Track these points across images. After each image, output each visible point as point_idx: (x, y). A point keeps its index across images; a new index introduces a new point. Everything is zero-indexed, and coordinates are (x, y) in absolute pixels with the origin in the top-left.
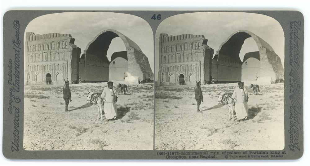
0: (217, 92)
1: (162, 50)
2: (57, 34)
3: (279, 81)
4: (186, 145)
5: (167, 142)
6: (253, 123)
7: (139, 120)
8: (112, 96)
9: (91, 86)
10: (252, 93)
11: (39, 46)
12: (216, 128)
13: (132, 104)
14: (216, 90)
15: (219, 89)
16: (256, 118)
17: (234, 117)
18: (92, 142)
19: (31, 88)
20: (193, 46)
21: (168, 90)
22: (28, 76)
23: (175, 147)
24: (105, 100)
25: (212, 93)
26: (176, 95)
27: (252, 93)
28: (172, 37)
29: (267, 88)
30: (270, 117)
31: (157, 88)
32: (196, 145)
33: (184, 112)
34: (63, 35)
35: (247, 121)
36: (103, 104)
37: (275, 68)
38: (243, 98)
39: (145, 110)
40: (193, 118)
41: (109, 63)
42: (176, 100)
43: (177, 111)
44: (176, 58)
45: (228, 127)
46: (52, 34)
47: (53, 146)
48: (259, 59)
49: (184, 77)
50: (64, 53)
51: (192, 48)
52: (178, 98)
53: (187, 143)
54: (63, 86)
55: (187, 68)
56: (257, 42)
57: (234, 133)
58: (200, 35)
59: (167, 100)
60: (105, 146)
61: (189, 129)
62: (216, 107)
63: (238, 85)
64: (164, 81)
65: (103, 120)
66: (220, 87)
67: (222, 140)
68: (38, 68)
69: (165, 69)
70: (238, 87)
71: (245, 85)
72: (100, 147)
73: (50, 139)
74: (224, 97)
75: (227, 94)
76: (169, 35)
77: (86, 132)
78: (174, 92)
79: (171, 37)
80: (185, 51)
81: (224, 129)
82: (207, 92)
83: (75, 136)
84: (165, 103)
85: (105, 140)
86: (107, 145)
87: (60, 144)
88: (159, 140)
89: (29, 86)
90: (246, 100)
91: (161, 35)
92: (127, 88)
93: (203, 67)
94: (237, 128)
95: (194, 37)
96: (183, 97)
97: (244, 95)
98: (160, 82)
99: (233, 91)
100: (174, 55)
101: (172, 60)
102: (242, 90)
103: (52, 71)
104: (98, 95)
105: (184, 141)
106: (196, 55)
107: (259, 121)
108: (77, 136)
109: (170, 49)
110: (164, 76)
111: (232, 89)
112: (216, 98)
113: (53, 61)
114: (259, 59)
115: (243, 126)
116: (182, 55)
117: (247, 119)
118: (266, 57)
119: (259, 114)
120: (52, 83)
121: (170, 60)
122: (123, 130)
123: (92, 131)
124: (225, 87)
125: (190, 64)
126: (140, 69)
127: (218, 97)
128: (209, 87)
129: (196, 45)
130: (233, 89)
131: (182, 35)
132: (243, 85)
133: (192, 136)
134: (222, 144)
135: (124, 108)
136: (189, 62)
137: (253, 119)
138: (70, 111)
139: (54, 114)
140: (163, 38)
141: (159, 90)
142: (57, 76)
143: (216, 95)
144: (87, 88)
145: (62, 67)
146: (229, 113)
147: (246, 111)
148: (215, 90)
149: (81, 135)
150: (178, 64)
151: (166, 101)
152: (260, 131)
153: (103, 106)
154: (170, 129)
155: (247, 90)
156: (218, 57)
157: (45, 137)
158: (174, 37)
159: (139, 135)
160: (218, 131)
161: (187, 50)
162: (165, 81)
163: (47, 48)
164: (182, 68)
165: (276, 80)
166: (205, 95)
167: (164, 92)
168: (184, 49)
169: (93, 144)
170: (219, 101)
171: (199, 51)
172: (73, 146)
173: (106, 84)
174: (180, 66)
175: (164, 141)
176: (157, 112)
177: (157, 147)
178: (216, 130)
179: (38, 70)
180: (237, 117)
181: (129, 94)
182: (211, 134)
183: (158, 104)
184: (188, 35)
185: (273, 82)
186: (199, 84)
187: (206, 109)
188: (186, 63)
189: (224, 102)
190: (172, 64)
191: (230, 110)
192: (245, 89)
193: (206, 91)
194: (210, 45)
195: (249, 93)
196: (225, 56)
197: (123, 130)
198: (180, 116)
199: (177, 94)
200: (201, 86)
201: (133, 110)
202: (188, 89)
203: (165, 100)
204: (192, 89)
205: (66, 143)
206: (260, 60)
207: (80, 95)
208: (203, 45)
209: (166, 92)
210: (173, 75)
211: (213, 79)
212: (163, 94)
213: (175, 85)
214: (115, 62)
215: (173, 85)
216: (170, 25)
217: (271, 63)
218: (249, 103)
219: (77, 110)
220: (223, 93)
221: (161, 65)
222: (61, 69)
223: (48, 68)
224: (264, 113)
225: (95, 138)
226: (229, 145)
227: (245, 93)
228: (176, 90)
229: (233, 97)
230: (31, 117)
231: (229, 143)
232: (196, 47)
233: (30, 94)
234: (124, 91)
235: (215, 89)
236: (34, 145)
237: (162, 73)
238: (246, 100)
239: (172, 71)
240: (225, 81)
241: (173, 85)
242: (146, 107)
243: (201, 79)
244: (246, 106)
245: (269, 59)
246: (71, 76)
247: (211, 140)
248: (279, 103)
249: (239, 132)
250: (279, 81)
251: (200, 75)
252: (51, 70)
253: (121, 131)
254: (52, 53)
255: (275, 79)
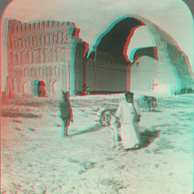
0: (94, 108)
1: (11, 44)
2: (54, 23)
3: (186, 91)
4: (47, 186)
5: (19, 182)
6: (147, 155)
7: (173, 150)
8: (132, 113)
9: (103, 99)
10: (145, 110)
11: (27, 40)
12: (92, 162)
13: (164, 126)
14: (93, 105)
15: (96, 103)
16: (153, 146)
17: (120, 145)
18: (102, 183)
19: (15, 102)
20: (58, 38)
21: (20, 104)
22: (11, 84)
23: (32, 190)
24: (122, 119)
25: (87, 109)
26: (33, 112)
27: (145, 110)
28: (27, 25)
29: (36, 103)
30: (172, 144)
31: (5, 101)
32: (63, 187)
33: (44, 137)
34: (63, 24)
35: (138, 150)
36: (119, 126)
37: (180, 71)
38: (132, 116)
39: (182, 134)
40: (57, 146)
41: (129, 64)
42: (32, 120)
43: (33, 136)
44: (33, 57)
45: (111, 159)
46: (38, 24)
47: (44, 189)
48: (157, 59)
49: (44, 85)
50: (64, 50)
51: (57, 42)
52: (36, 117)
53: (48, 184)
54: (60, 99)
55: (49, 72)
56: (153, 34)
57: (119, 169)
58: (68, 23)
59: (19, 119)
60: (121, 188)
61: (51, 162)
62: (92, 130)
63: (125, 97)
64: (15, 91)
65: (120, 150)
66: (99, 99)
67: (101, 179)
68: (25, 73)
69: (16, 72)
70: (125, 100)
71: (135, 97)
72: (114, 189)
73: (40, 179)
74: (104, 115)
75: (108, 110)
76: (22, 23)
77: (93, 167)
78: (29, 108)
79: (25, 25)
80: (46, 47)
81: (104, 163)
82: (79, 107)
83: (77, 173)
84: (16, 123)
85: (122, 179)
86: (125, 186)
87: (55, 186)
88: (8, 180)
89: (13, 100)
90: (137, 119)
91: (10, 22)
92: (157, 103)
93: (73, 70)
94: (124, 161)
95: (59, 26)
96: (42, 114)
97: (133, 111)
98: (9, 92)
99: (118, 106)
100: (30, 52)
101: (27, 60)
102: (130, 105)
103: (46, 77)
104: (111, 112)
105: (45, 180)
106: (62, 51)
107: (157, 151)
108: (80, 173)
109: (24, 43)
110: (15, 83)
111: (116, 104)
112: (91, 116)
113: (47, 63)
114: (157, 59)
115: (133, 158)
116: (41, 52)
117: (138, 148)
118: (167, 54)
119: (157, 140)
120: (46, 95)
121: (24, 60)
122: (149, 164)
123: (103, 166)
124: (105, 100)
125: (54, 64)
126: (176, 73)
127: (96, 115)
128: (81, 101)
129: (63, 37)
130: (117, 104)
131: (41, 22)
132: (132, 97)
133: (56, 173)
134: (101, 185)
135: (152, 132)
136: (52, 62)
137: (147, 148)
138: (71, 136)
139: (48, 141)
140: (13, 27)
141: (7, 104)
142: (54, 84)
143: (92, 112)
144: (96, 103)
145: (61, 71)
146: (112, 139)
147: (137, 135)
148: (91, 104)
149: (86, 171)
150: (35, 65)
151: (17, 122)
152: (157, 166)
153: (119, 128)
154: (24, 164)
155: (138, 104)
156: (95, 55)
157: (33, 175)
158: (30, 25)
159: (172, 172)
160: (95, 165)
161: (49, 45)
162: (16, 92)
163: (39, 44)
164: (41, 72)
165: (182, 90)
166: (76, 112)
167: (15, 107)
168: (45, 43)
169: (104, 186)
170: (96, 121)
171: (67, 46)
172: (74, 188)
173: (123, 96)
174: (38, 68)
175: (15, 182)
176: (4, 138)
177: (5, 190)
178: (92, 164)
179: (25, 76)
180: (124, 144)
181: (160, 110)
182: (84, 170)
183: (6, 125)
184: (51, 22)
185: (177, 92)
186: (66, 95)
187: (77, 132)
188: (48, 64)
189: (104, 122)
190: (26, 66)
191: (113, 134)
192: (135, 103)
193: (77, 106)
194: (83, 37)
195: (141, 109)
196: (105, 54)
197: (149, 164)
198: (39, 143)
199: (35, 110)
200: (71, 98)
201: (165, 135)
202: (50, 103)
203: (16, 119)
204: (57, 104)
205: (64, 184)
206: (157, 60)
207: (87, 113)
208: (72, 38)
209: (18, 107)
210: (29, 81)
211: (88, 87)
212: (14, 110)
213: (32, 97)
214: (139, 63)
215: (29, 97)
216: (23, 7)
217: (175, 65)
218: (141, 124)
219: (82, 135)
220: (102, 109)
221: (11, 67)
222: (59, 75)
223: (40, 73)
224: (163, 139)
225: (107, 176)
226: (111, 186)
227: (135, 110)
228: (32, 104)
229: (117, 114)
230: (13, 145)
231: (111, 183)
232: (62, 40)
233: (14, 112)
234: (153, 105)
235: (90, 103)
236: (17, 187)
237: (11, 80)
238: (137, 119)
239: (27, 76)
240: (107, 90)
241: (29, 97)
242: (184, 129)
243: (69, 88)
244: (137, 129)
245: (172, 58)
246: (74, 84)
247: (85, 179)
248: (186, 123)
249: (126, 167)
250: (186, 91)
251: (68, 82)
252: (45, 76)
253: (146, 165)
254: (46, 51)
255: (180, 88)
